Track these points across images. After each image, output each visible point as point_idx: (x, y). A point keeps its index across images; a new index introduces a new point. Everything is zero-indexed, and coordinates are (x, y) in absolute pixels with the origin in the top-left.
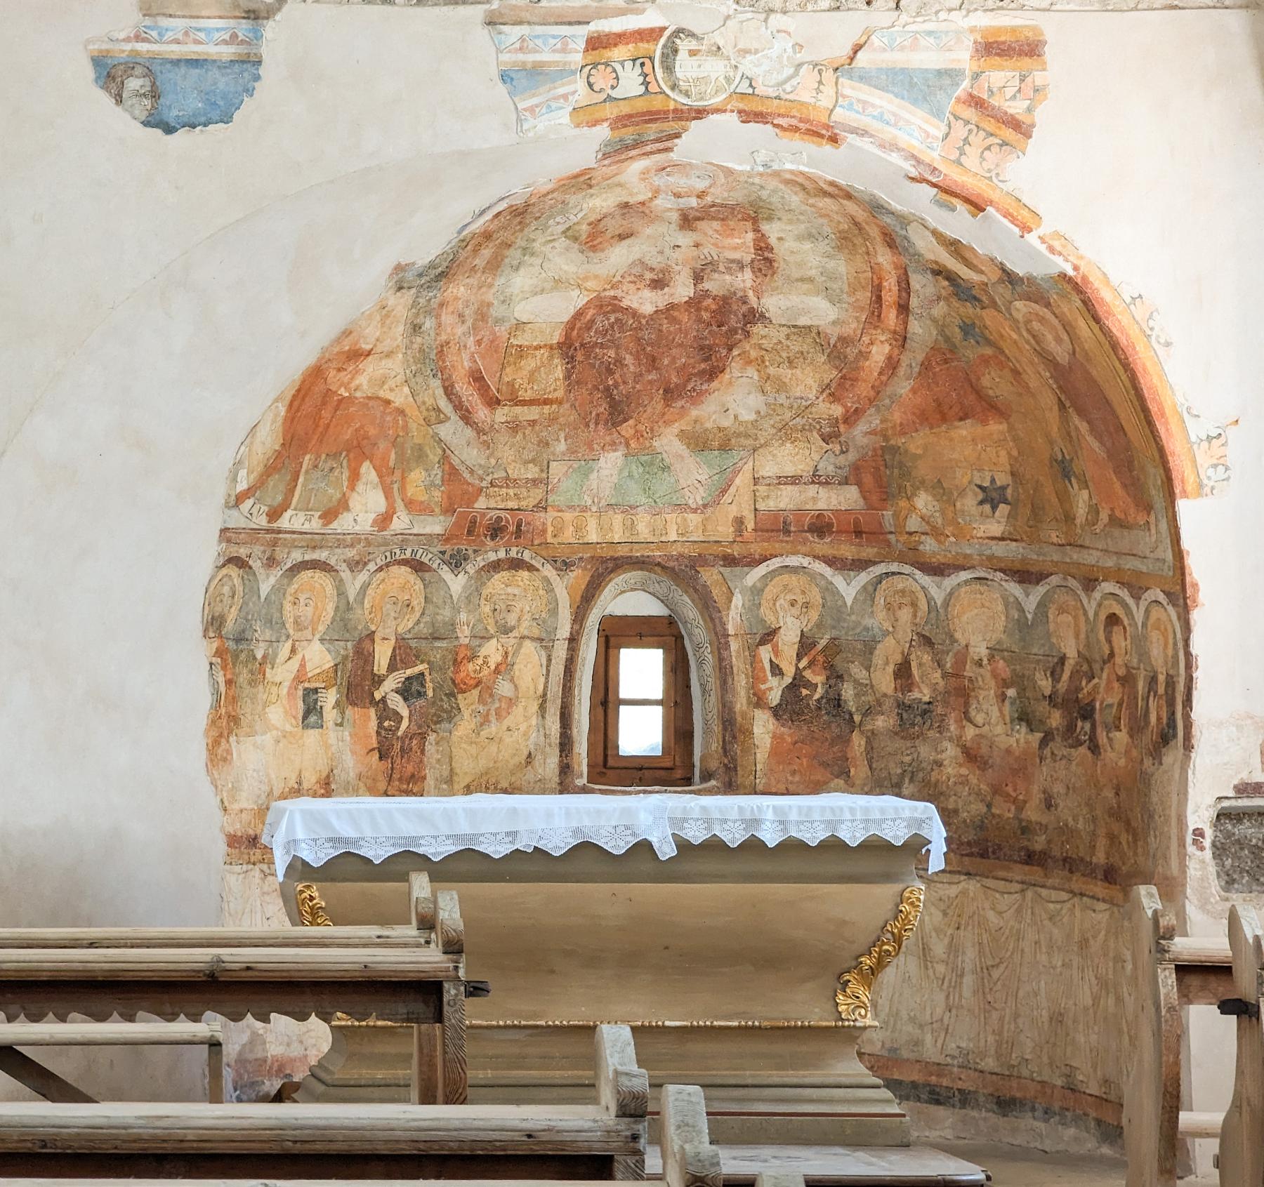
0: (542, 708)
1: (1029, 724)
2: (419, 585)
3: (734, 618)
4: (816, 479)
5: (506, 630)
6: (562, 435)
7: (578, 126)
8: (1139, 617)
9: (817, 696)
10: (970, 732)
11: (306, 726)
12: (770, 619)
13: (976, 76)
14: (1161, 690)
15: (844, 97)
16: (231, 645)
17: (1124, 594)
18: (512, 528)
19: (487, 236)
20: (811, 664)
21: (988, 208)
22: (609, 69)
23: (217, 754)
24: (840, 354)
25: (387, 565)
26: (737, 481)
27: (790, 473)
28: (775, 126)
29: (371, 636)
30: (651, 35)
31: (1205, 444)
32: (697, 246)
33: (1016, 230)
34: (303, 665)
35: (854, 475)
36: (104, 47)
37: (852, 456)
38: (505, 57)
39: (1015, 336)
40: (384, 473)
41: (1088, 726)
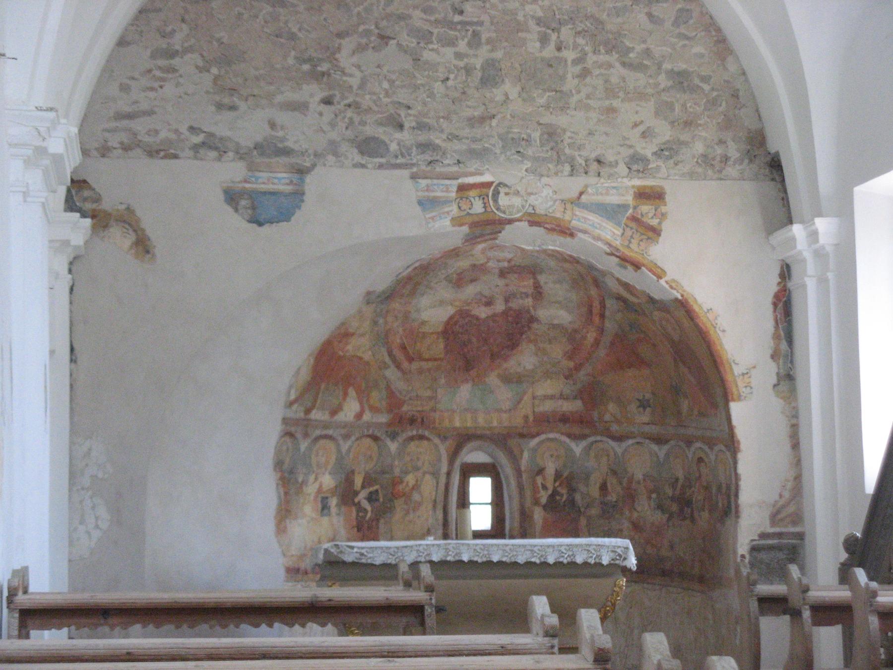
0: (434, 507)
1: (662, 510)
2: (376, 448)
3: (524, 462)
4: (562, 397)
5: (416, 469)
7: (454, 226)
8: (713, 457)
10: (635, 515)
11: (322, 515)
12: (541, 463)
13: (635, 208)
14: (724, 490)
16: (286, 475)
17: (706, 448)
18: (419, 420)
19: (409, 278)
20: (560, 485)
23: (281, 529)
24: (573, 336)
25: (361, 437)
26: (525, 398)
27: (550, 394)
28: (547, 228)
29: (353, 472)
30: (488, 185)
32: (507, 285)
33: (655, 278)
34: (321, 486)
35: (579, 395)
37: (579, 386)
38: (420, 194)
41: (689, 510)
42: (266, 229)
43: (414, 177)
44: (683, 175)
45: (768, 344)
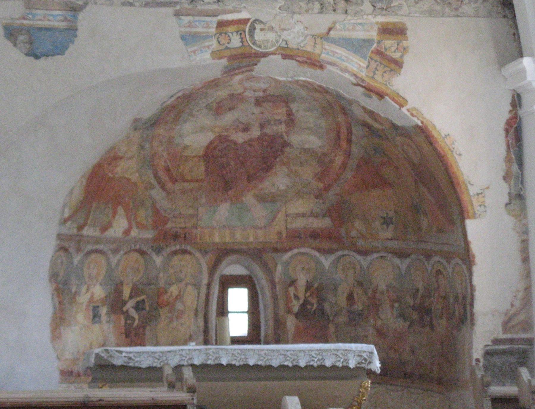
0: (196, 315)
1: (404, 318)
2: (142, 262)
4: (313, 215)
5: (180, 280)
6: (204, 196)
7: (213, 59)
8: (450, 270)
9: (314, 308)
10: (380, 322)
11: (94, 322)
12: (293, 276)
13: (379, 42)
15: (325, 49)
16: (61, 286)
17: (444, 261)
18: (182, 236)
19: (173, 107)
20: (311, 295)
21: (386, 97)
22: (227, 36)
24: (322, 160)
25: (129, 252)
26: (279, 216)
27: (302, 212)
28: (297, 61)
29: (121, 283)
30: (245, 21)
31: (476, 197)
32: (262, 113)
33: (397, 106)
34: (92, 296)
35: (328, 213)
36: (10, 21)
37: (328, 205)
38: (183, 29)
39: (397, 152)
40: (128, 210)
42: (43, 62)
43: (177, 14)
44: (423, 12)
45: (500, 166)
